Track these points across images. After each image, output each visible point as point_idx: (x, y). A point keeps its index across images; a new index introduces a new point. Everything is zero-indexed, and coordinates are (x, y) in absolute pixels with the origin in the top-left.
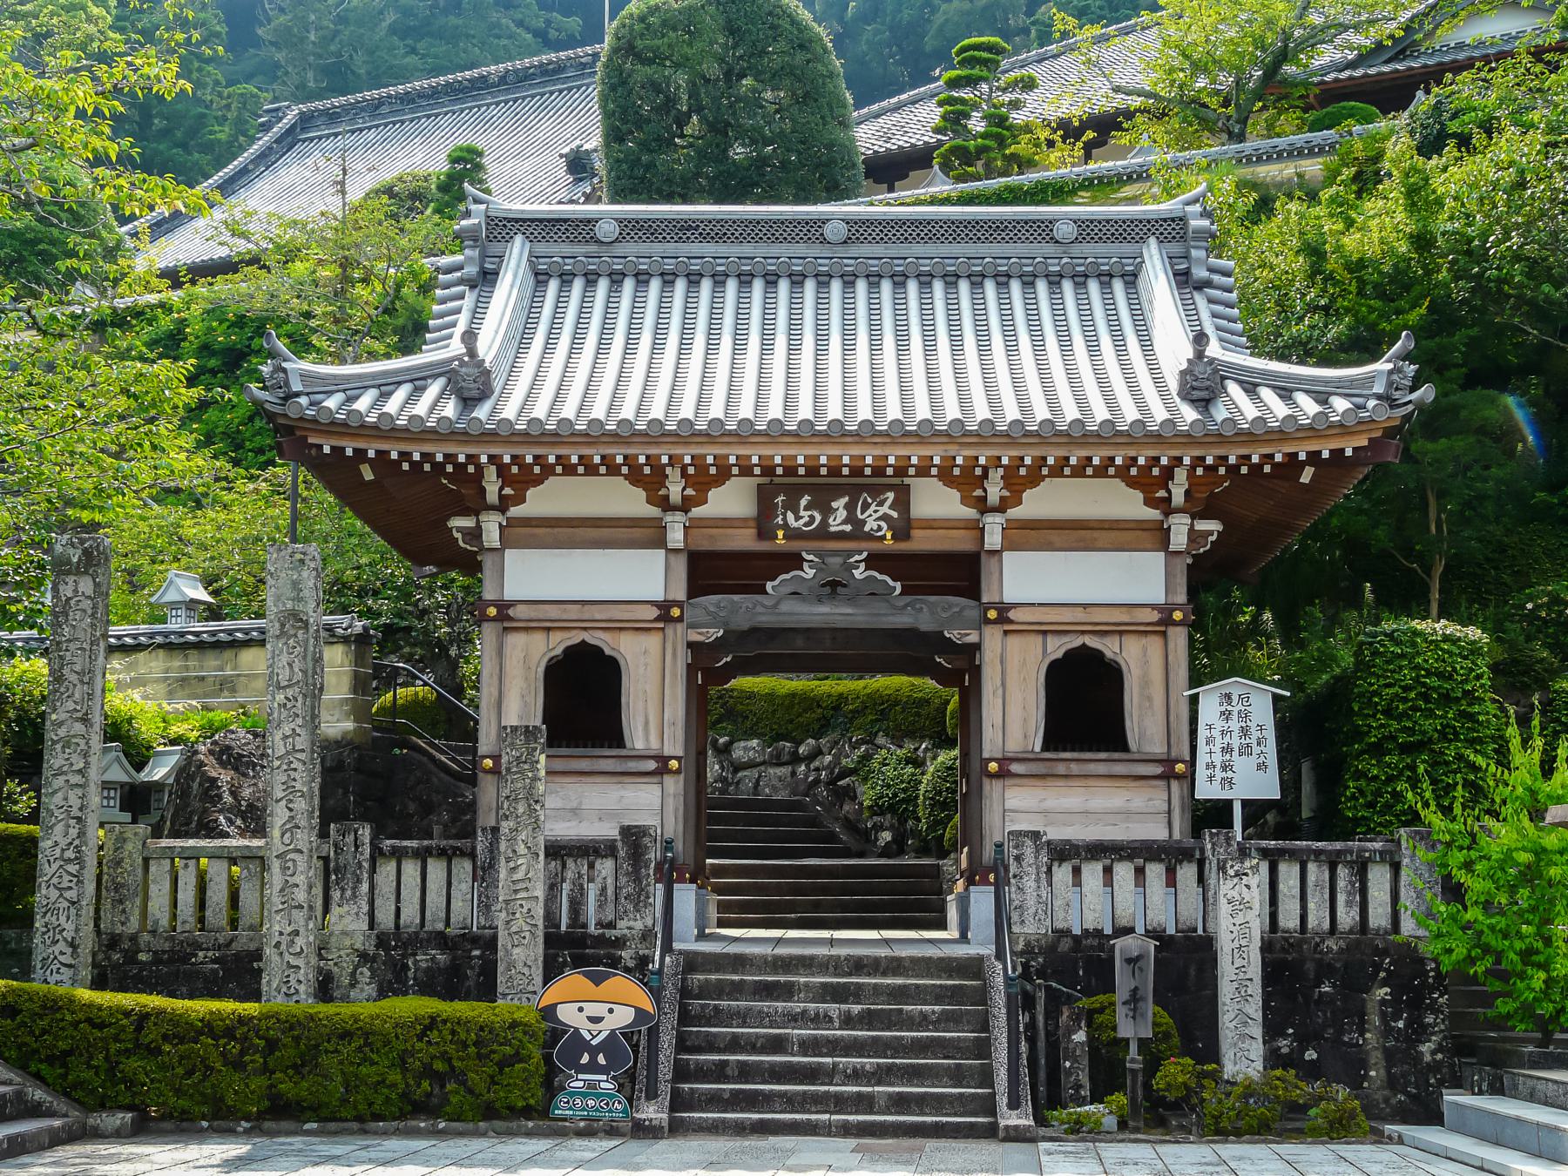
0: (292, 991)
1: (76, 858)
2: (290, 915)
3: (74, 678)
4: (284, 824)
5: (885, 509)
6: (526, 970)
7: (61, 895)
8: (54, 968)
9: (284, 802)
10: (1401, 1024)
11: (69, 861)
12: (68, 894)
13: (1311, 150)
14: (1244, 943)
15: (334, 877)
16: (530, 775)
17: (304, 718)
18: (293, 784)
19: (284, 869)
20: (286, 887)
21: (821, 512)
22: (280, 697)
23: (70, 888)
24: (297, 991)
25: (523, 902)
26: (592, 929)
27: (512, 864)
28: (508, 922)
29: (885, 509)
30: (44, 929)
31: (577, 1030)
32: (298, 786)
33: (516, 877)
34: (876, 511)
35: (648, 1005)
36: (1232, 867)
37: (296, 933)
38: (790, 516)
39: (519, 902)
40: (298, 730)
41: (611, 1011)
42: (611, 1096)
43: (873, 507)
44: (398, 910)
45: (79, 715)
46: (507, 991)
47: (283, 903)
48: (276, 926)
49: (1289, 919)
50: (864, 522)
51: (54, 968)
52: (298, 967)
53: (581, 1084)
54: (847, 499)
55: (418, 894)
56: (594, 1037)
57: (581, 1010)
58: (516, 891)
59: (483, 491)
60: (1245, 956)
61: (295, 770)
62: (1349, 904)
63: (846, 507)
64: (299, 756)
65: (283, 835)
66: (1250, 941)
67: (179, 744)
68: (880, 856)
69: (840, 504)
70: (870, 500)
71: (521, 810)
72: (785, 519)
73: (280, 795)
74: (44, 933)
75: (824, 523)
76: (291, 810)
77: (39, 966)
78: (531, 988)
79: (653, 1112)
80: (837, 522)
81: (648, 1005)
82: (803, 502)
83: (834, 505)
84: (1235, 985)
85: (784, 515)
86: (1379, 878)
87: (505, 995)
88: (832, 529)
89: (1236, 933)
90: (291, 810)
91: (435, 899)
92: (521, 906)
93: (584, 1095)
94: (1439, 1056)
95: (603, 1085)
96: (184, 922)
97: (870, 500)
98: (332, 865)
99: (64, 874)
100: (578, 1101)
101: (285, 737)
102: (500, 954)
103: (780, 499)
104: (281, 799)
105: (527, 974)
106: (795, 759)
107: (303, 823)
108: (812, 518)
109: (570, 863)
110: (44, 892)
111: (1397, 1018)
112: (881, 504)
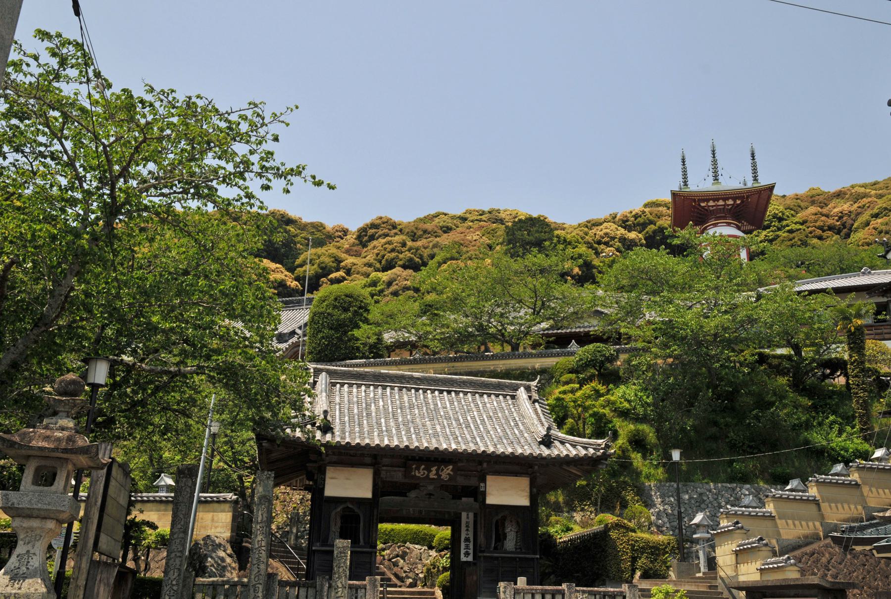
3: (181, 516)
5: (449, 471)
19: (255, 590)
44: (307, 592)
54: (436, 467)
68: (408, 587)
73: (255, 562)
75: (428, 475)
82: (423, 467)
101: (259, 541)
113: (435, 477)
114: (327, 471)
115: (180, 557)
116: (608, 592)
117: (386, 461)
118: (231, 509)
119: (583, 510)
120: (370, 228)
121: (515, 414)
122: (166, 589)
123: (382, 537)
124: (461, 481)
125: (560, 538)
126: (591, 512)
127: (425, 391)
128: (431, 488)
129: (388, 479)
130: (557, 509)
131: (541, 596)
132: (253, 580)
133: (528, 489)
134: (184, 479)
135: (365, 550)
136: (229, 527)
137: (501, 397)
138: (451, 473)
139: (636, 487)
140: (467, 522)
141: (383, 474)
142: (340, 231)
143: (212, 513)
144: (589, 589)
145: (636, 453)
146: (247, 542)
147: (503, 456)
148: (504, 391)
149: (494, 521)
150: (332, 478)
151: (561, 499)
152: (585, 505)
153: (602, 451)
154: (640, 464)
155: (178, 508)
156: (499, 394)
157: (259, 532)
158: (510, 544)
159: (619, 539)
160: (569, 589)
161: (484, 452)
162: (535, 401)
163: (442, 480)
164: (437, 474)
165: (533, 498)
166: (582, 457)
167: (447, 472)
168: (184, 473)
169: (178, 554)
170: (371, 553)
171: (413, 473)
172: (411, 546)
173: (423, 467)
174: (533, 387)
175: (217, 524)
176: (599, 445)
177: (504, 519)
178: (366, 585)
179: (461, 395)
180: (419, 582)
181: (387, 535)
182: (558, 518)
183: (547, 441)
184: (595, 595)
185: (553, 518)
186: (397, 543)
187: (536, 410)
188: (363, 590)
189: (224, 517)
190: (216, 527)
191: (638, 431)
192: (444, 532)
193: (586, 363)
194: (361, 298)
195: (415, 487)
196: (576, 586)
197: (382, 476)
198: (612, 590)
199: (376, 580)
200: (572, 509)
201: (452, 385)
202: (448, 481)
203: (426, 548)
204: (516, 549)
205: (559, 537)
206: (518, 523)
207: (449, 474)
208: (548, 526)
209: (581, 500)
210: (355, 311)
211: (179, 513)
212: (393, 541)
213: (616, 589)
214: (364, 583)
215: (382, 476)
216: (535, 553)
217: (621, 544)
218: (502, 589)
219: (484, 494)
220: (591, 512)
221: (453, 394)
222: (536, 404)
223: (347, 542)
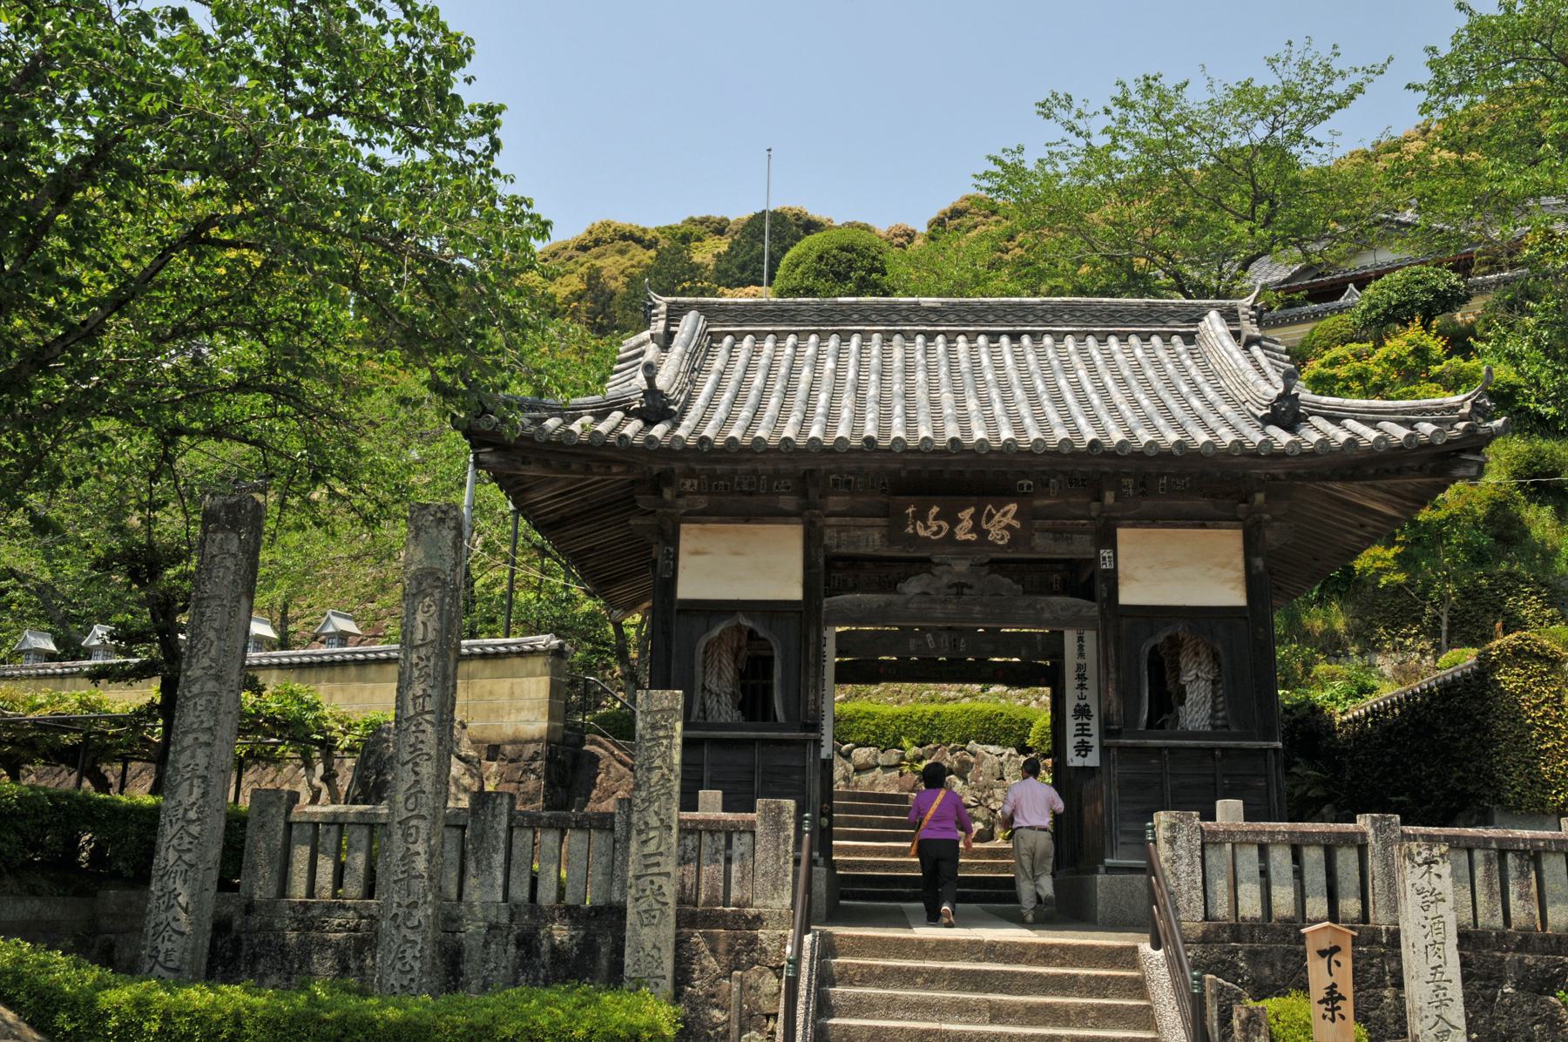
0: (408, 968)
1: (198, 819)
3: (212, 635)
4: (409, 789)
5: (1008, 520)
6: (654, 953)
7: (180, 857)
8: (166, 935)
9: (410, 765)
11: (190, 822)
12: (186, 857)
13: (1300, 318)
14: (1439, 939)
17: (435, 678)
18: (420, 746)
19: (406, 836)
21: (949, 523)
23: (189, 850)
25: (654, 878)
27: (643, 837)
30: (160, 893)
37: (414, 905)
39: (650, 878)
45: (212, 672)
46: (633, 975)
47: (403, 872)
51: (166, 935)
52: (415, 942)
54: (972, 510)
58: (647, 866)
60: (1441, 953)
61: (424, 731)
63: (972, 517)
64: (428, 717)
65: (407, 799)
72: (915, 529)
73: (407, 757)
74: (159, 898)
75: (951, 533)
76: (416, 774)
77: (151, 932)
78: (659, 972)
80: (963, 533)
82: (935, 510)
85: (914, 524)
89: (1428, 929)
90: (416, 774)
92: (652, 882)
99: (185, 835)
101: (415, 698)
102: (628, 934)
103: (910, 510)
104: (408, 762)
105: (656, 956)
108: (940, 528)
110: (162, 853)
112: (1004, 515)
113: (973, 537)
114: (683, 536)
115: (208, 744)
116: (1516, 840)
117: (835, 502)
118: (548, 669)
119: (1401, 648)
120: (950, 218)
121: (1194, 371)
122: (170, 831)
123: (917, 732)
124: (1044, 546)
125: (1343, 714)
126: (1423, 653)
127: (951, 339)
128: (961, 566)
129: (843, 550)
130: (1333, 647)
131: (1288, 852)
132: (400, 806)
133: (1239, 561)
134: (220, 536)
135: (786, 735)
136: (545, 709)
137: (1155, 340)
138: (1016, 524)
139: (1544, 585)
140: (1079, 667)
141: (830, 538)
142: (902, 236)
143: (510, 680)
144: (1448, 831)
145: (1534, 506)
146: (593, 742)
147: (1152, 453)
148: (1164, 324)
149: (1145, 649)
150: (697, 553)
151: (1340, 624)
152: (1406, 636)
153: (1461, 425)
154: (1551, 533)
155: (203, 614)
156: (1152, 334)
157: (416, 673)
158: (1196, 712)
159: (1525, 692)
160: (1379, 831)
161: (1094, 443)
162: (1251, 342)
163: (993, 544)
164: (976, 528)
165: (1252, 583)
166: (1401, 447)
167: (1003, 521)
168: (216, 520)
169: (204, 738)
170: (803, 743)
171: (910, 530)
172: (979, 748)
173: (935, 510)
174: (1241, 310)
175: (520, 704)
176: (1453, 409)
177: (1175, 644)
178: (753, 823)
179: (1048, 340)
180: (998, 830)
181: (925, 726)
182: (1334, 667)
183: (1286, 413)
184: (1470, 851)
185: (1321, 668)
186: (948, 744)
187: (1254, 361)
188: (747, 838)
189: (534, 687)
190: (519, 710)
191: (1538, 453)
192: (1034, 705)
193: (1385, 311)
194: (874, 252)
195: (923, 564)
196: (1403, 823)
197: (826, 541)
198: (1527, 834)
199: (781, 810)
200: (1371, 647)
201: (1023, 319)
202: (1009, 545)
203: (1013, 751)
204: (1214, 726)
205: (1339, 709)
206: (1215, 657)
207: (1008, 527)
208: (1308, 686)
209: (1395, 625)
210: (862, 279)
211: (205, 627)
212: (940, 737)
213: (1539, 833)
214: (750, 816)
215: (826, 541)
216: (1269, 737)
217: (1536, 707)
218: (1162, 833)
219: (1112, 578)
220: (1423, 653)
221: (1026, 340)
222: (1255, 349)
223: (673, 698)
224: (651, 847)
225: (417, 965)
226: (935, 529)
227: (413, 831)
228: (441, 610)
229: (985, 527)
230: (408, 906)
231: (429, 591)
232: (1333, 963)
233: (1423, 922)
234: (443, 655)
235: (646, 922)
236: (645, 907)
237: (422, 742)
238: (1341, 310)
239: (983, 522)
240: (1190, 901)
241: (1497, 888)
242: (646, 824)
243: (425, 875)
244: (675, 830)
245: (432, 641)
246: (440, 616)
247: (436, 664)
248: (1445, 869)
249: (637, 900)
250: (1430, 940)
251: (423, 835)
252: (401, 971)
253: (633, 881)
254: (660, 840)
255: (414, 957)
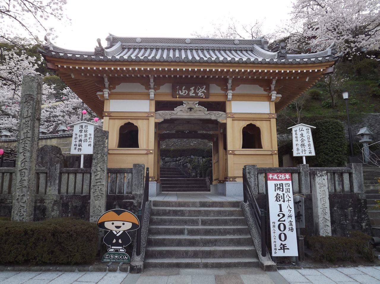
2: (22, 190)
6: (99, 208)
9: (22, 154)
10: (356, 218)
15: (48, 179)
16: (102, 146)
17: (31, 127)
18: (26, 148)
20: (22, 181)
22: (24, 121)
24: (23, 215)
26: (125, 194)
28: (94, 192)
29: (203, 90)
31: (111, 231)
32: (27, 148)
33: (97, 178)
34: (201, 91)
35: (136, 222)
36: (319, 173)
38: (180, 91)
39: (98, 186)
40: (29, 131)
41: (123, 224)
42: (124, 254)
43: (200, 89)
46: (93, 215)
48: (17, 193)
49: (338, 188)
50: (198, 93)
53: (113, 250)
55: (73, 184)
56: (117, 233)
57: (113, 224)
59: (105, 85)
62: (339, 184)
64: (28, 139)
66: (326, 196)
67: (238, 207)
69: (192, 89)
70: (199, 88)
71: (99, 157)
72: (179, 92)
73: (22, 151)
75: (188, 94)
76: (24, 156)
79: (138, 261)
81: (136, 222)
82: (183, 88)
83: (191, 89)
84: (322, 209)
86: (346, 177)
87: (92, 216)
88: (190, 95)
89: (321, 194)
90: (24, 156)
91: (79, 185)
93: (114, 254)
94: (367, 227)
95: (121, 250)
96: (5, 191)
97: (199, 88)
98: (48, 175)
100: (112, 256)
105: (100, 209)
106: (176, 161)
107: (28, 160)
109: (118, 175)
111: (355, 216)
164: (195, 92)
188: (130, 175)
224: (98, 177)
225: (25, 214)
226: (184, 92)
227: (23, 173)
228: (33, 107)
229: (198, 92)
230: (22, 196)
231: (29, 101)
232: (299, 206)
233: (320, 192)
234: (33, 120)
235: (96, 199)
236: (96, 195)
237: (26, 146)
238: (160, 159)
239: (197, 91)
240: (254, 189)
241: (333, 182)
242: (97, 170)
243: (27, 186)
244: (106, 172)
245: (30, 116)
246: (33, 108)
247: (31, 123)
248: (325, 177)
249: (94, 192)
250: (322, 197)
251: (27, 174)
252: (20, 216)
253: (93, 187)
254: (101, 175)
255: (24, 211)
